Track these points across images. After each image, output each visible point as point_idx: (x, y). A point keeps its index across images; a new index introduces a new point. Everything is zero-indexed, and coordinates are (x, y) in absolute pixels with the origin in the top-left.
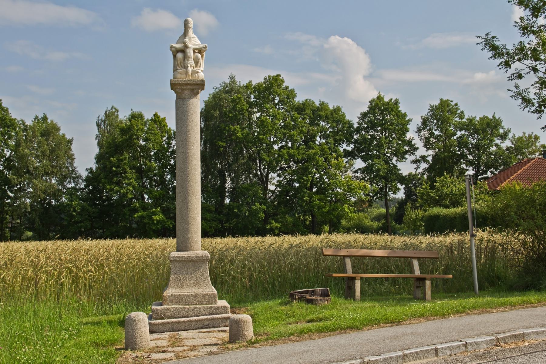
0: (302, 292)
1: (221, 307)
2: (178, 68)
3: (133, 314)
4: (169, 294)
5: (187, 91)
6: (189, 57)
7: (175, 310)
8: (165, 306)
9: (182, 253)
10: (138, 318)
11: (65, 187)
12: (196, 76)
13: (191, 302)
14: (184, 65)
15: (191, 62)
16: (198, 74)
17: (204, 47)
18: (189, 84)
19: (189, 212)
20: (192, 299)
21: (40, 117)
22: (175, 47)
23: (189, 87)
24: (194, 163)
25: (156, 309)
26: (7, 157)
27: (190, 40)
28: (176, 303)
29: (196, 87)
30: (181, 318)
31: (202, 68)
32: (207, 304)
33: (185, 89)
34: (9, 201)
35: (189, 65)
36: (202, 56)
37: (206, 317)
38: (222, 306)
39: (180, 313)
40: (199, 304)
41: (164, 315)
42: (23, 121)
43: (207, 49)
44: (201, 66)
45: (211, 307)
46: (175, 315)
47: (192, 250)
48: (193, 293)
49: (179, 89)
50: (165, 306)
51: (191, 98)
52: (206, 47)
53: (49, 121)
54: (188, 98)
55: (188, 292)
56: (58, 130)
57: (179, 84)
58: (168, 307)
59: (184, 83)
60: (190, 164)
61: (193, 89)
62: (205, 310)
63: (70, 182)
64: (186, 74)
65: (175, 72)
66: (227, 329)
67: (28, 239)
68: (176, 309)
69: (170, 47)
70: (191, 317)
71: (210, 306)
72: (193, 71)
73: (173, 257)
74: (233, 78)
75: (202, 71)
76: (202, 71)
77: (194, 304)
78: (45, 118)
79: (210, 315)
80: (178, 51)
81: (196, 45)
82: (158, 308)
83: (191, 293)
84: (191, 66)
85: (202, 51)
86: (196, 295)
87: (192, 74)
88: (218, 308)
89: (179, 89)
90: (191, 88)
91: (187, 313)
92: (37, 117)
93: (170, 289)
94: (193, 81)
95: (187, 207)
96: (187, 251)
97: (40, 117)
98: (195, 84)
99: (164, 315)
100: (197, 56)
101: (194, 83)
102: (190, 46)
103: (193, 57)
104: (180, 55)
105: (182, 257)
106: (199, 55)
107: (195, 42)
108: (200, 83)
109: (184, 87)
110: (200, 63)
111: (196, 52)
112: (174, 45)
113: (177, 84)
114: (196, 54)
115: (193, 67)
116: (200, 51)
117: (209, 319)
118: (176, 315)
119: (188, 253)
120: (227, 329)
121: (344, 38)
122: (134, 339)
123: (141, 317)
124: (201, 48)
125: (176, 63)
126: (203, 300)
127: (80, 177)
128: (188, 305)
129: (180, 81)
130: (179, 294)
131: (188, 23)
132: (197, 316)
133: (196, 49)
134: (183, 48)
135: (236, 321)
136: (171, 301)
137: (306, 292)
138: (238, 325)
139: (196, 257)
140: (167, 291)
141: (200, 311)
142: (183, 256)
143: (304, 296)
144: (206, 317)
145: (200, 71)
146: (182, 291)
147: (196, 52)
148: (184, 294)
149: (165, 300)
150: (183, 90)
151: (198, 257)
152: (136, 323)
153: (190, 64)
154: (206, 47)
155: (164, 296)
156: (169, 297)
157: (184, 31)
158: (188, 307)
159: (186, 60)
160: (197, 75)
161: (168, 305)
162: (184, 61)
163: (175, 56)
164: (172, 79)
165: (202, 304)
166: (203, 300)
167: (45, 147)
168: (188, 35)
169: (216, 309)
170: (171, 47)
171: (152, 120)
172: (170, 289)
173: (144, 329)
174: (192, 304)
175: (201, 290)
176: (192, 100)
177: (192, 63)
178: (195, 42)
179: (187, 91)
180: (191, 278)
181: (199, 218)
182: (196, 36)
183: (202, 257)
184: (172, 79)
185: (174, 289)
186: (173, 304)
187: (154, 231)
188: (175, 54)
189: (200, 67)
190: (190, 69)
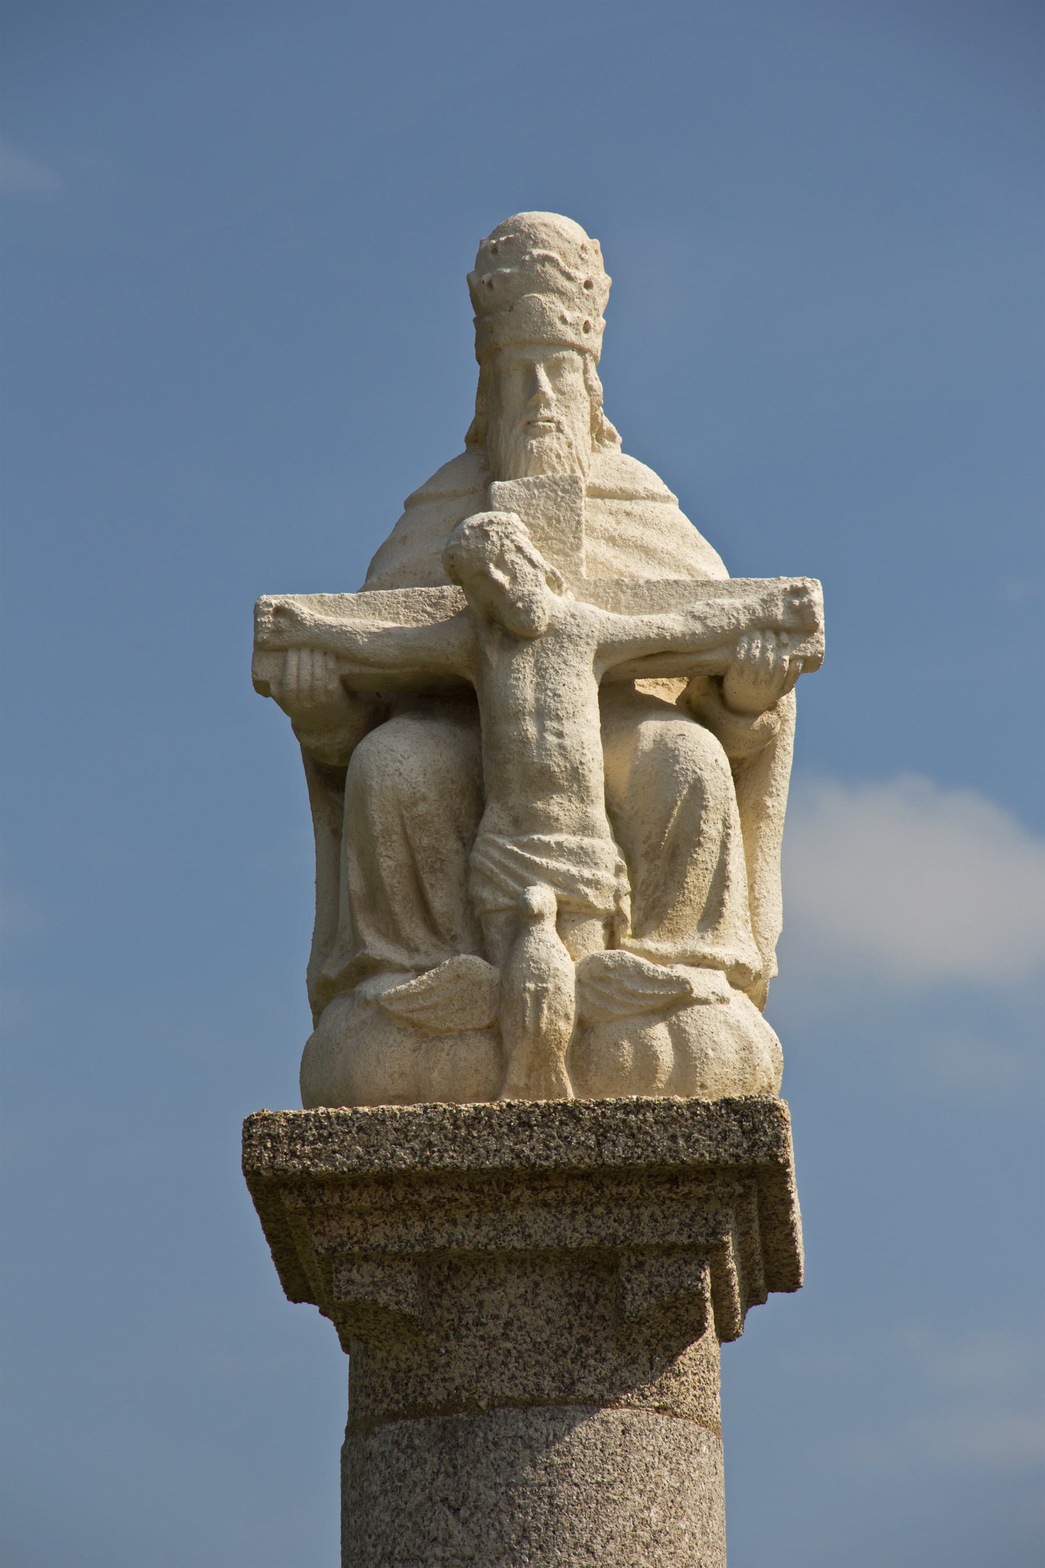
2: (377, 947)
12: (647, 1056)
14: (470, 903)
16: (690, 1018)
17: (765, 626)
38: (241, 1138)
43: (819, 643)
44: (736, 898)
49: (379, 1257)
54: (531, 1403)
57: (386, 1179)
64: (494, 1032)
65: (339, 1011)
69: (261, 647)
74: (453, 566)
85: (737, 688)
87: (583, 1026)
89: (379, 1257)
94: (602, 1131)
101: (616, 1152)
103: (596, 780)
107: (647, 552)
110: (707, 856)
111: (654, 707)
114: (651, 728)
116: (718, 681)
121: (604, 317)
124: (731, 637)
125: (354, 880)
129: (403, 1132)
147: (654, 707)
153: (563, 883)
159: (494, 815)
160: (660, 1035)
162: (468, 839)
168: (538, 461)
178: (647, 552)
179: (516, 1287)
182: (650, 479)
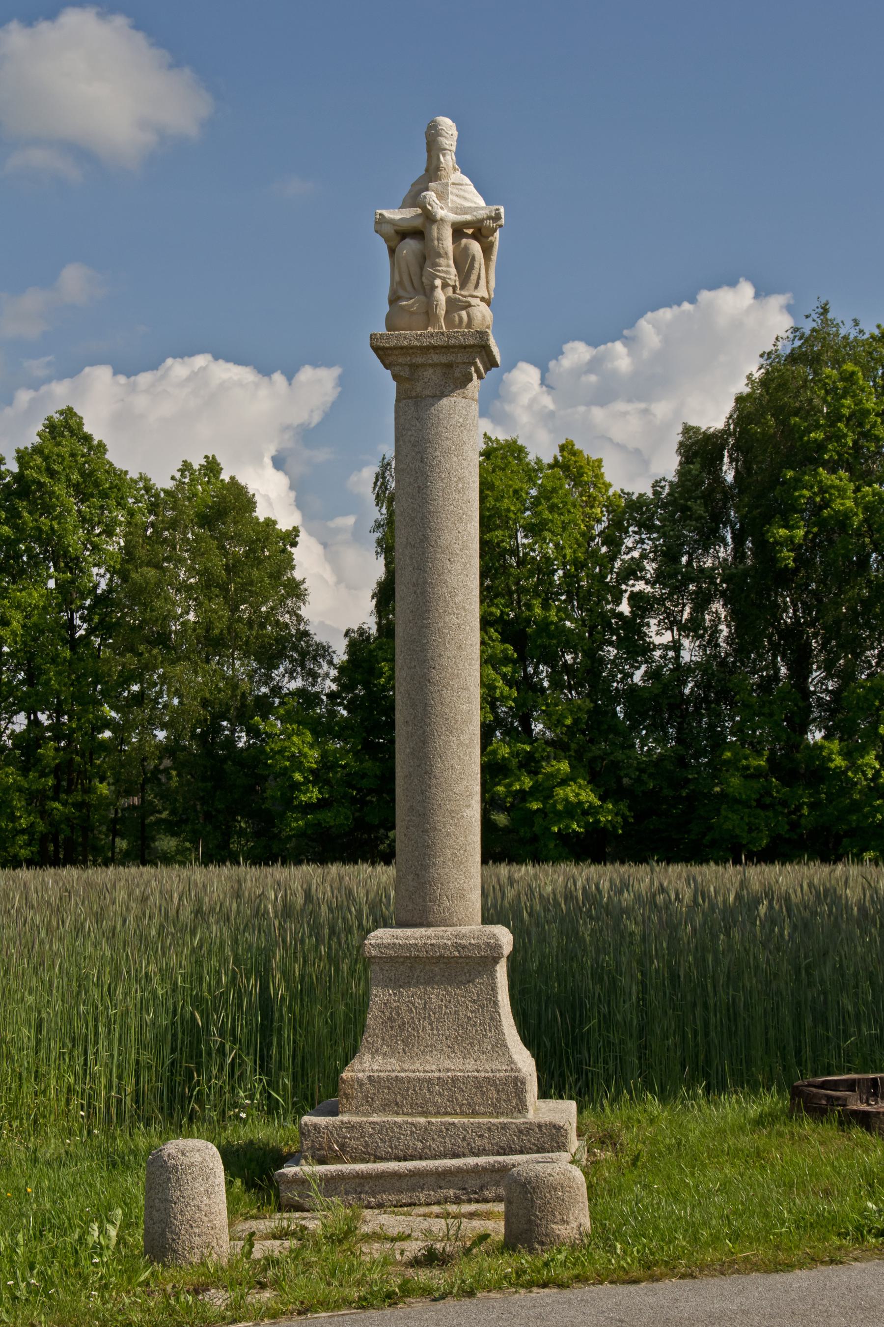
0: (835, 1085)
1: (540, 1126)
3: (173, 1147)
4: (360, 1075)
5: (429, 373)
6: (439, 255)
7: (380, 1132)
8: (345, 1118)
9: (409, 932)
10: (186, 1161)
11: (276, 690)
13: (435, 1104)
15: (449, 269)
17: (489, 218)
18: (434, 347)
19: (434, 790)
20: (440, 1095)
21: (196, 467)
22: (391, 222)
23: (435, 358)
24: (455, 620)
25: (316, 1127)
26: (99, 591)
27: (442, 196)
28: (385, 1108)
29: (461, 357)
30: (398, 1159)
31: (482, 292)
32: (491, 1115)
33: (423, 365)
34: (107, 734)
35: (438, 282)
36: (487, 250)
37: (482, 1160)
39: (395, 1142)
40: (463, 1114)
41: (342, 1147)
42: (146, 480)
45: (504, 1127)
46: (378, 1147)
47: (445, 923)
48: (442, 1075)
50: (345, 1118)
51: (442, 395)
52: (497, 217)
53: (225, 476)
54: (434, 397)
55: (428, 1068)
56: (249, 504)
57: (402, 348)
58: (355, 1119)
59: (416, 343)
60: (441, 624)
61: (450, 366)
62: (481, 1136)
63: (291, 674)
66: (500, 1207)
67: (167, 859)
68: (382, 1127)
70: (435, 1157)
71: (501, 1120)
72: (449, 300)
73: (379, 946)
75: (483, 299)
76: (483, 299)
77: (446, 1114)
78: (212, 467)
79: (499, 1154)
80: (403, 233)
81: (464, 211)
82: (322, 1121)
83: (437, 1074)
84: (445, 285)
85: (484, 232)
86: (454, 1080)
88: (526, 1130)
90: (444, 359)
91: (420, 1145)
92: (186, 467)
93: (367, 1057)
95: (429, 773)
96: (429, 925)
97: (196, 467)
98: (454, 347)
99: (342, 1147)
100: (466, 248)
101: (452, 342)
102: (441, 212)
103: (451, 255)
104: (409, 247)
105: (409, 947)
106: (476, 247)
107: (465, 198)
108: (472, 341)
109: (419, 360)
112: (387, 214)
113: (395, 348)
114: (464, 241)
115: (454, 287)
117: (484, 1169)
118: (384, 1149)
119: (430, 931)
120: (500, 1207)
122: (169, 1236)
123: (197, 1158)
124: (482, 221)
126: (478, 1099)
127: (323, 651)
128: (424, 1114)
130: (393, 1075)
131: (438, 134)
132: (456, 1156)
133: (467, 224)
134: (418, 223)
135: (524, 1185)
136: (368, 1100)
137: (851, 1086)
138: (532, 1200)
139: (457, 946)
140: (355, 1063)
141: (464, 1139)
142: (412, 941)
143: (838, 1098)
144: (482, 1160)
145: (473, 301)
146: (406, 1067)
148: (412, 1075)
149: (347, 1096)
150: (414, 367)
151: (464, 947)
152: (178, 1180)
154: (497, 217)
155: (344, 1081)
156: (361, 1084)
157: (424, 166)
158: (422, 1120)
159: (428, 262)
160: (464, 313)
161: (357, 1114)
162: (422, 268)
163: (392, 251)
164: (383, 330)
165: (475, 1114)
166: (478, 1099)
167: (218, 563)
169: (521, 1132)
170: (381, 221)
171: (555, 464)
172: (367, 1057)
173: (206, 1200)
174: (438, 1114)
175: (470, 1064)
176: (445, 401)
177: (447, 272)
178: (465, 198)
179: (431, 371)
180: (438, 1020)
181: (473, 812)
183: (478, 946)
184: (383, 330)
185: (380, 1058)
186: (375, 1111)
187: (564, 838)
188: (392, 244)
189: (477, 286)
190: (441, 296)
